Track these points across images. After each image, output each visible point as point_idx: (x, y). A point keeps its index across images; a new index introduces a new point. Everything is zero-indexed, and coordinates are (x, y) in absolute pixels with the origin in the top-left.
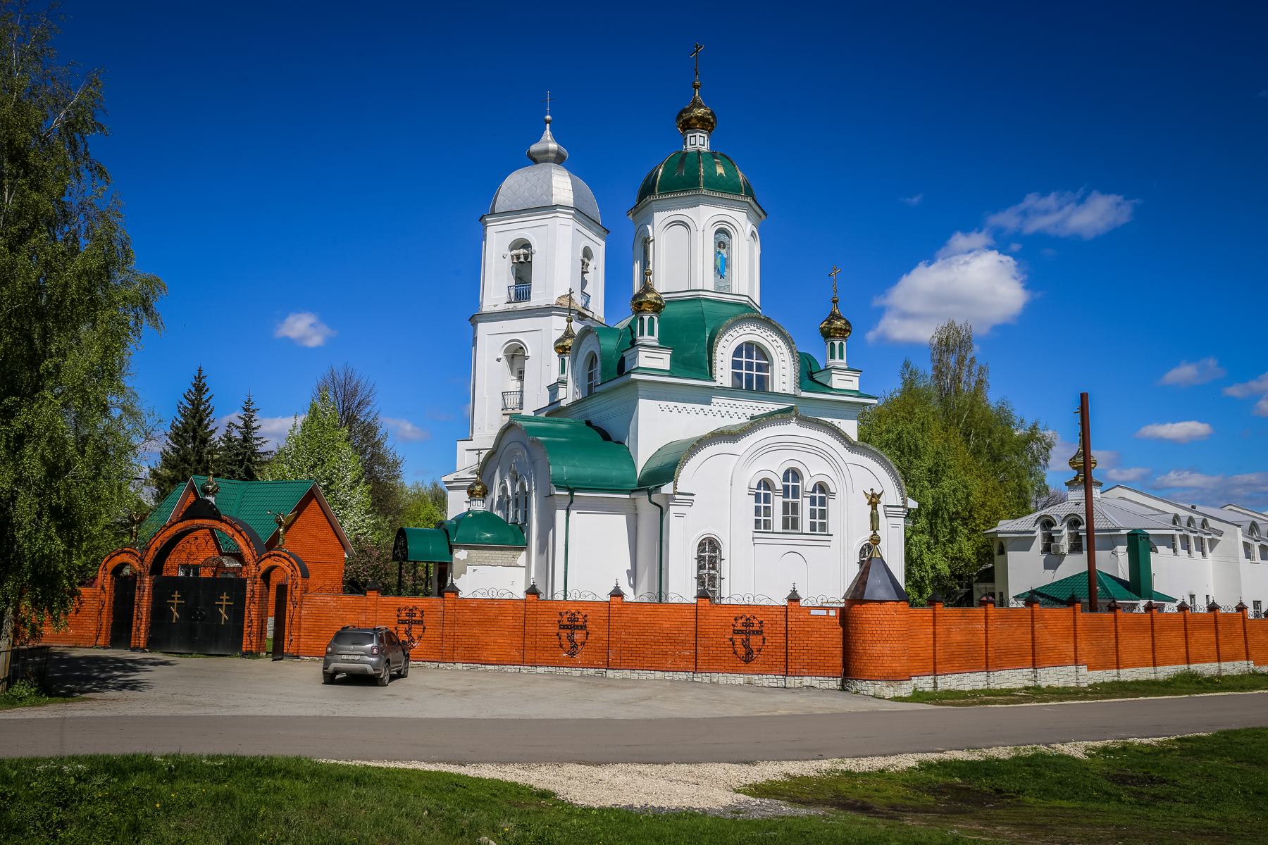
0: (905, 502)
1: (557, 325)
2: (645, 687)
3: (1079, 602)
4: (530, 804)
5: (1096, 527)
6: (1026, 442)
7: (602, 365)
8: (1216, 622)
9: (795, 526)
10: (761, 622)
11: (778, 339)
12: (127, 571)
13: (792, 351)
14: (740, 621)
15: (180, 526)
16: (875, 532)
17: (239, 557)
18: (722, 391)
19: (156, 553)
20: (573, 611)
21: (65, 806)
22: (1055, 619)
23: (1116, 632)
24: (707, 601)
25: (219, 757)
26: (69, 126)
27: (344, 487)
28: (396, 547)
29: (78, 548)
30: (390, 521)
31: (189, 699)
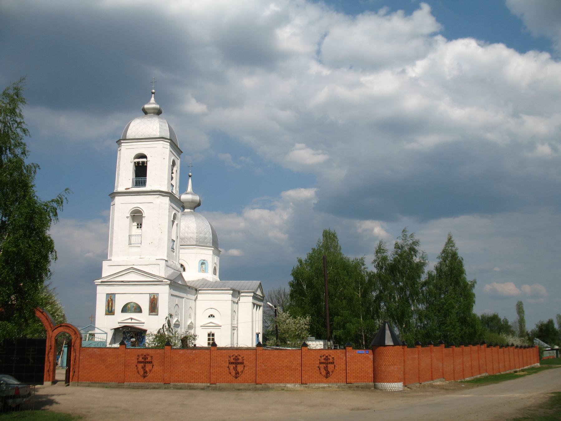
10: (333, 358)
14: (323, 358)
20: (236, 355)
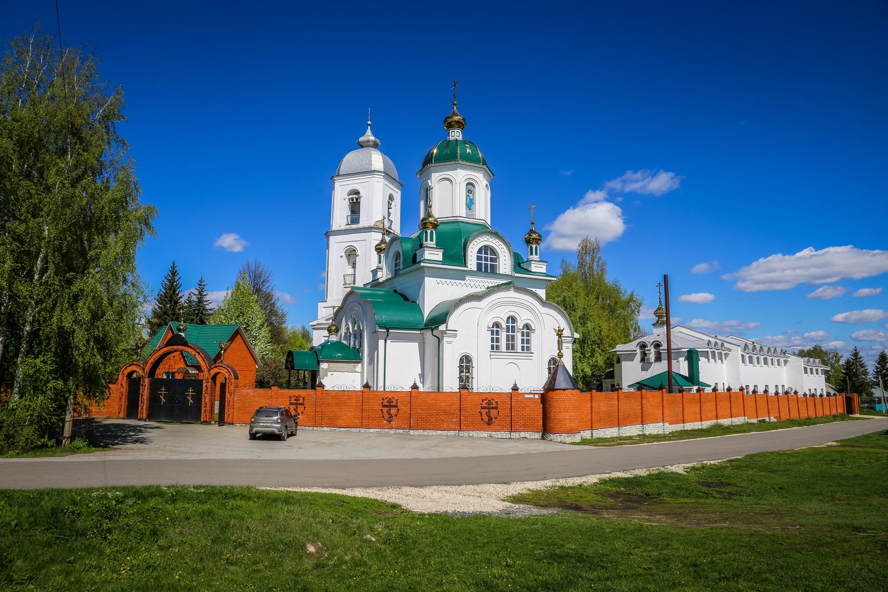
0: (573, 334)
1: (377, 237)
2: (432, 440)
3: (665, 388)
4: (388, 512)
5: (672, 348)
6: (628, 302)
7: (404, 258)
8: (730, 397)
9: (513, 348)
11: (502, 244)
12: (134, 376)
13: (509, 251)
14: (485, 402)
15: (165, 350)
16: (560, 351)
17: (198, 368)
18: (471, 273)
19: (152, 365)
20: (390, 397)
21: (110, 518)
22: (652, 397)
23: (683, 404)
24: (466, 391)
25: (201, 487)
26: (106, 118)
27: (255, 328)
28: (287, 361)
29: (109, 361)
30: (281, 347)
31: (174, 449)
